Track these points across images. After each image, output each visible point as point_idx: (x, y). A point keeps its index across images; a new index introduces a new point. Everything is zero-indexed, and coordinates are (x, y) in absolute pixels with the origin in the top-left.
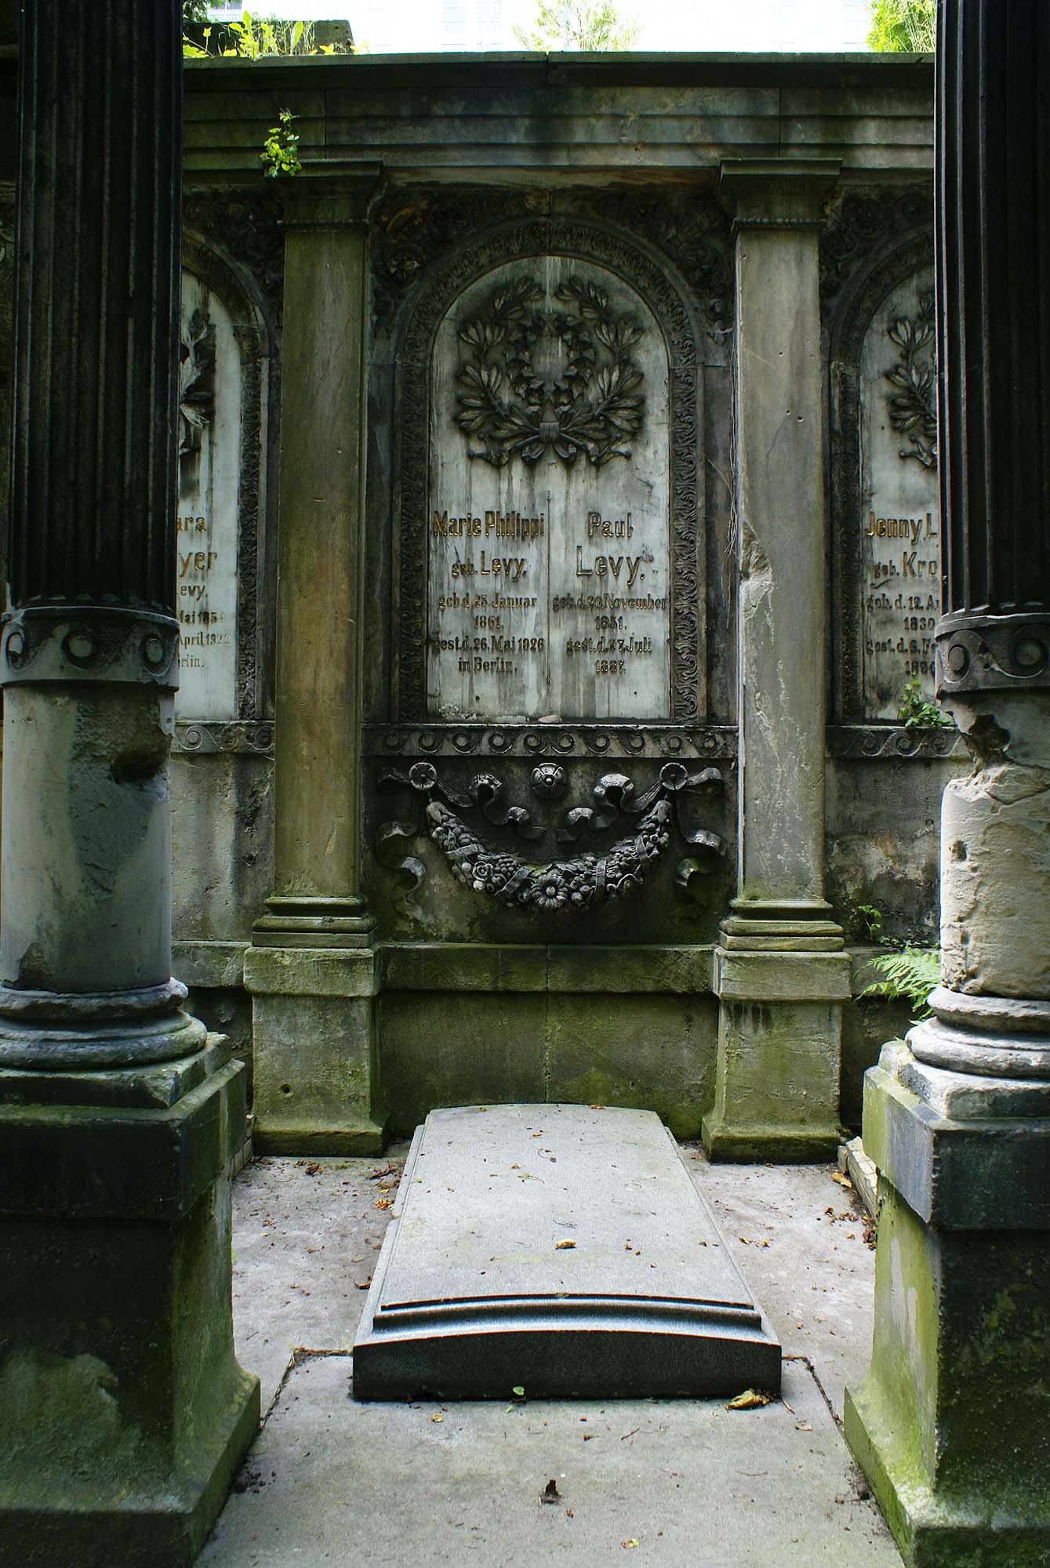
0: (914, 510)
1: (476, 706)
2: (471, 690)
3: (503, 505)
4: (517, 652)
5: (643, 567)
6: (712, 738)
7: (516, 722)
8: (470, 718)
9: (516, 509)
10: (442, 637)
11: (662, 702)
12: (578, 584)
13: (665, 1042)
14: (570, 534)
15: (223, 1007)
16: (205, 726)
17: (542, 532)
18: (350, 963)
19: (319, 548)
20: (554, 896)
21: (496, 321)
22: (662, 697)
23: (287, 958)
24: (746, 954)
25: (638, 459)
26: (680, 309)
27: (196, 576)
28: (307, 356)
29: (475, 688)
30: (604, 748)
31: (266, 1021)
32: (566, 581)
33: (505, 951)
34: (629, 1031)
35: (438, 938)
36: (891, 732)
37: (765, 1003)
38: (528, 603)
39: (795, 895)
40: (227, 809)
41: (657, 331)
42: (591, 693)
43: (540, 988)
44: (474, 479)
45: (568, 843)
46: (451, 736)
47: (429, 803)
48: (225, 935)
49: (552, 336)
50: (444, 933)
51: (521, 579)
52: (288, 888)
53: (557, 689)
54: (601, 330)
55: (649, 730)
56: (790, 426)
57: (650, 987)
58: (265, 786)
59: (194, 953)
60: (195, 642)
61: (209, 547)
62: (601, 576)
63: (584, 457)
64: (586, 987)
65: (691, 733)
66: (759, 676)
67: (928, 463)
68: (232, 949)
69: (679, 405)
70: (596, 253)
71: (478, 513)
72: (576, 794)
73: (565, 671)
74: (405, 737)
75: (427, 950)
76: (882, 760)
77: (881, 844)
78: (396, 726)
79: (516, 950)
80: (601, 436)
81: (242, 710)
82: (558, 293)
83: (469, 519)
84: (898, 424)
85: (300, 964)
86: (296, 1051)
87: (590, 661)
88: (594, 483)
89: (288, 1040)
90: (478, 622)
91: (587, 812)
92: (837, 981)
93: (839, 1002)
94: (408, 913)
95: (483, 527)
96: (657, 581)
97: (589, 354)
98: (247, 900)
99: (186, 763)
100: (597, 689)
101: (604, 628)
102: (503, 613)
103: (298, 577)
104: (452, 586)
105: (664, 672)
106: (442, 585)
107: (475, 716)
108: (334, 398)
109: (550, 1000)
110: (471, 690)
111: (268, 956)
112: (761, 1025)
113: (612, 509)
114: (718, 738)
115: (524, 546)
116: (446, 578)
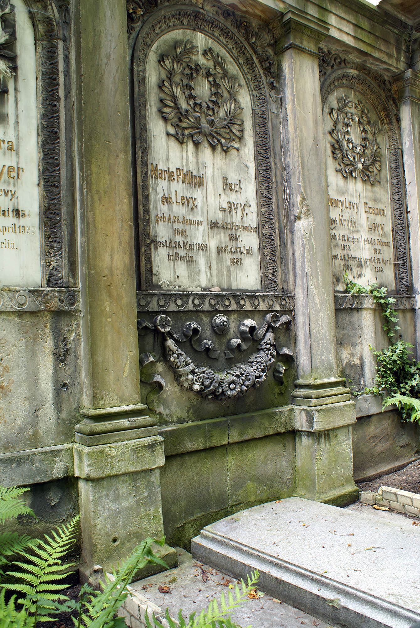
0: (341, 196)
1: (178, 282)
2: (175, 272)
3: (185, 166)
4: (195, 250)
5: (247, 210)
6: (285, 299)
7: (198, 291)
8: (175, 289)
9: (191, 169)
10: (159, 239)
11: (258, 281)
12: (220, 215)
13: (276, 460)
14: (216, 187)
15: (52, 494)
16: (30, 291)
17: (203, 184)
18: (151, 446)
19: (110, 174)
20: (234, 389)
21: (177, 59)
22: (257, 278)
23: (114, 450)
24: (322, 407)
25: (242, 152)
26: (259, 80)
27: (9, 183)
28: (97, 47)
29: (176, 271)
30: (243, 305)
31: (100, 497)
32: (215, 213)
33: (209, 424)
34: (262, 458)
35: (172, 422)
36: (346, 297)
37: (328, 430)
38: (198, 223)
39: (329, 376)
40: (46, 351)
41: (246, 88)
42: (229, 276)
43: (225, 442)
44: (170, 148)
45: (230, 359)
46: (173, 299)
47: (167, 340)
48: (51, 442)
49: (203, 76)
50: (175, 419)
51: (195, 209)
52: (101, 402)
53: (214, 273)
54: (225, 80)
55: (261, 296)
56: (314, 148)
57: (271, 432)
58: (71, 333)
59: (32, 459)
60: (10, 230)
61: (18, 163)
62: (230, 212)
63: (219, 146)
64: (246, 437)
65: (277, 297)
66: (311, 268)
67: (345, 176)
68: (59, 451)
69: (258, 128)
70: (221, 39)
71: (173, 169)
72: (232, 331)
73: (217, 263)
74: (149, 299)
75: (171, 431)
76: (344, 309)
77: (346, 349)
78: (144, 293)
79: (214, 423)
80: (227, 136)
81: (49, 281)
82: (205, 53)
83: (169, 171)
84: (335, 155)
85: (123, 453)
86: (120, 512)
87: (228, 257)
88: (224, 161)
89: (114, 507)
90: (176, 232)
91: (239, 341)
92: (352, 415)
93: (351, 425)
94: (156, 409)
95: (175, 177)
96: (252, 219)
97: (220, 91)
98: (64, 415)
99: (16, 319)
100: (231, 273)
101: (233, 240)
102: (187, 227)
103: (98, 191)
104: (162, 209)
105: (258, 265)
106: (156, 208)
107: (177, 288)
108: (114, 78)
109: (228, 448)
110: (175, 272)
111: (102, 452)
112: (327, 441)
113: (233, 177)
114: (287, 299)
115: (195, 190)
116: (158, 203)
